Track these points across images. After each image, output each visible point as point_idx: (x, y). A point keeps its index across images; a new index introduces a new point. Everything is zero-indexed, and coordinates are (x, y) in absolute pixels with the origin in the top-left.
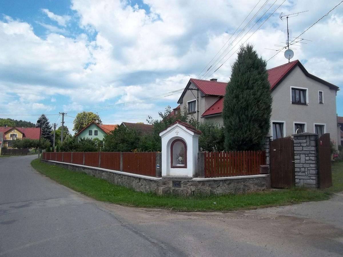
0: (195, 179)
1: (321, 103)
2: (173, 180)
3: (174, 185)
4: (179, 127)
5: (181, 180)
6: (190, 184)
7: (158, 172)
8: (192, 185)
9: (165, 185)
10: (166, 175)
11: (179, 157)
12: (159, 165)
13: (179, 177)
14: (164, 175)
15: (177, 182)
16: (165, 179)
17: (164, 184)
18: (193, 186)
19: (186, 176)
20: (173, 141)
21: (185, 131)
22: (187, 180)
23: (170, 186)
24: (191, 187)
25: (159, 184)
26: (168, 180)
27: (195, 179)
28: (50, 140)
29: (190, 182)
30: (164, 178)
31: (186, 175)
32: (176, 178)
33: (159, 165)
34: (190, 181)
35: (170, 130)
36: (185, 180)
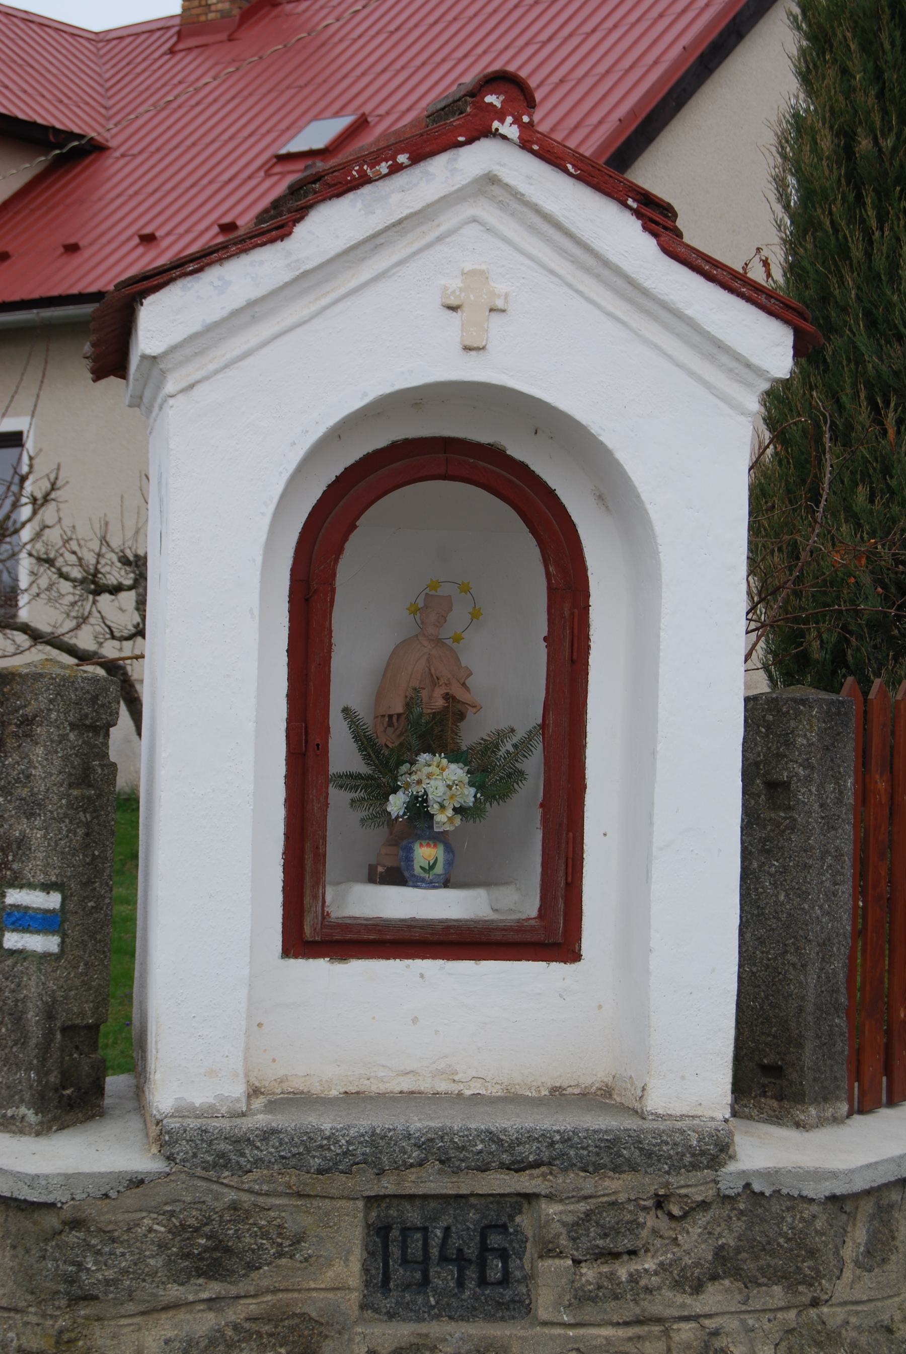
0: (767, 1152)
1: (491, 310)
2: (388, 1185)
3: (399, 1273)
4: (518, 197)
5: (525, 1183)
6: (694, 1242)
7: (36, 1034)
8: (736, 1273)
9: (215, 1288)
10: (237, 1090)
11: (430, 780)
12: (53, 901)
13: (492, 1137)
14: (200, 1096)
15: (451, 1217)
16: (222, 1162)
17: (209, 1254)
18: (750, 1282)
19: (558, 1096)
20: (349, 472)
21: (634, 291)
22: (650, 1183)
23: (313, 1304)
24: (714, 1298)
25: (95, 1272)
26: (293, 1178)
27: (767, 1152)
28: (467, 768)
29: (704, 1205)
30: (206, 1150)
31: (591, 1071)
32: (441, 1151)
33: (53, 901)
34: (698, 1195)
35: (354, 254)
36: (616, 1186)
